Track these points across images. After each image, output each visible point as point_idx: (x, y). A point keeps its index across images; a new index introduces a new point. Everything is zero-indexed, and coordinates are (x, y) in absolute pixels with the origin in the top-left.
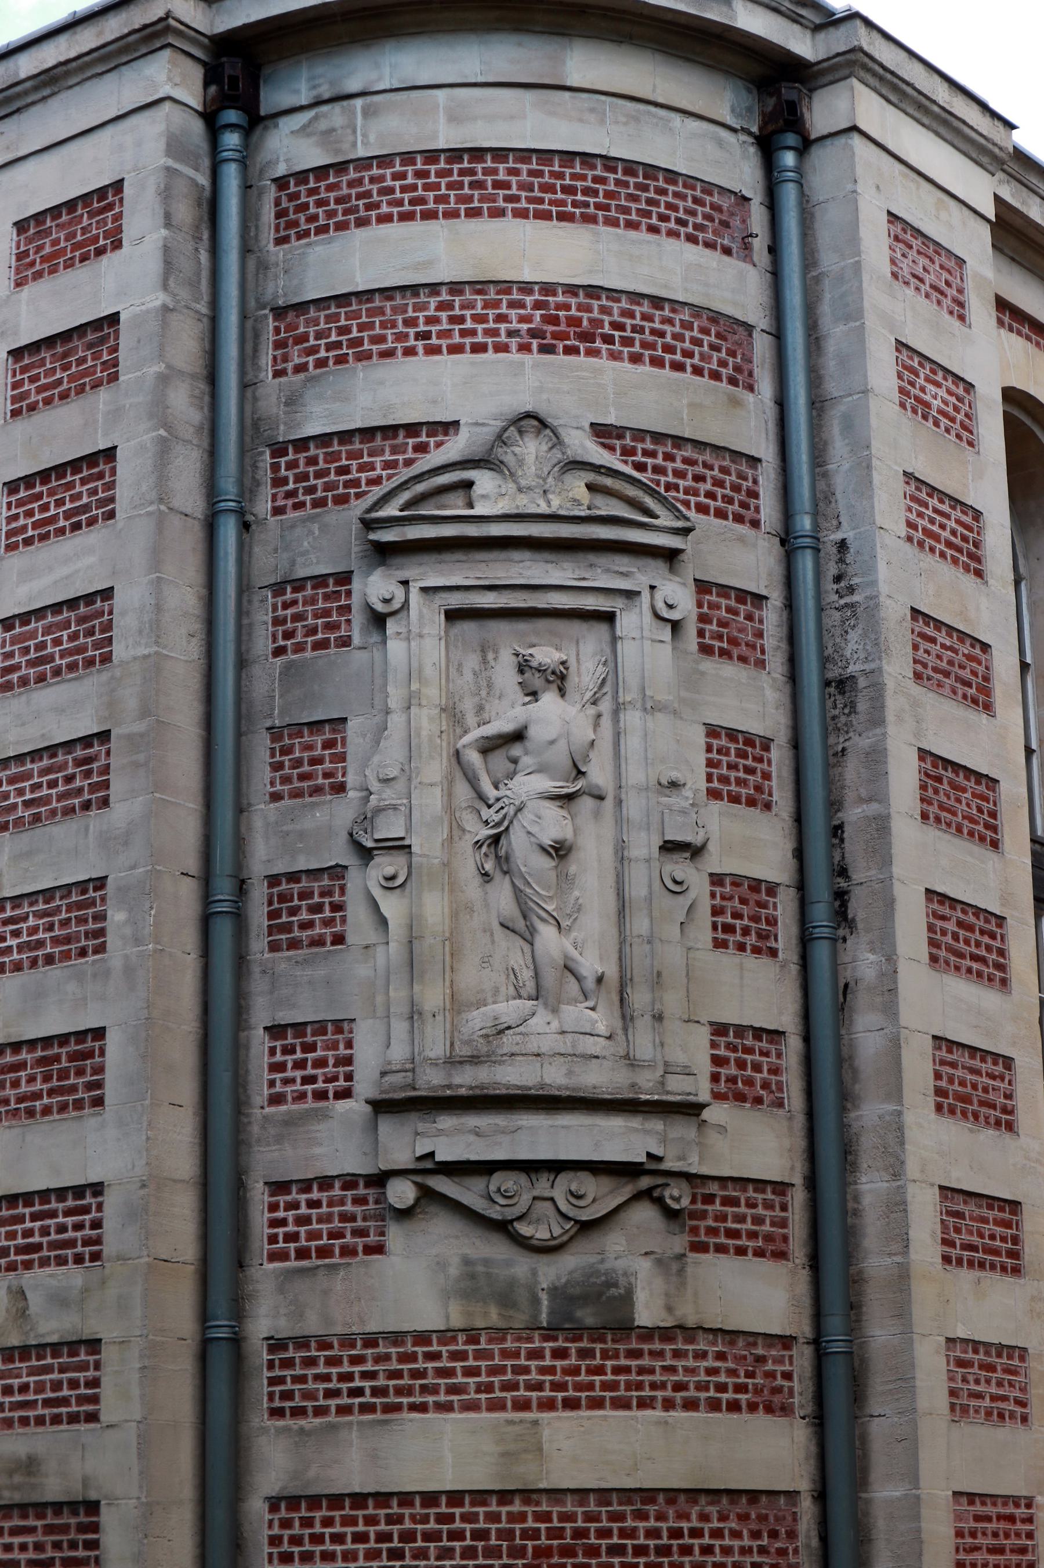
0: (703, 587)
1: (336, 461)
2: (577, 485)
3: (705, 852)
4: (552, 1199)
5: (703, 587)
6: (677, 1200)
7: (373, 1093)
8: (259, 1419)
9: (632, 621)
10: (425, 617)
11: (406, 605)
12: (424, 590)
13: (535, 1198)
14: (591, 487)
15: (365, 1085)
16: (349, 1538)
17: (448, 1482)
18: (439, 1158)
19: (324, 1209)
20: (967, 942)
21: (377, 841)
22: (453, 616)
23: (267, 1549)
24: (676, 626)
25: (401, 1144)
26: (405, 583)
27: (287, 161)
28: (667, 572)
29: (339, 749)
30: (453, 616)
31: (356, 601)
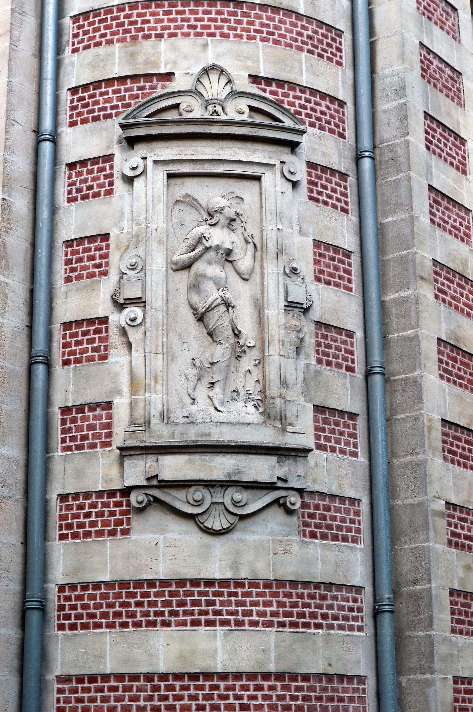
0: (311, 165)
1: (71, 247)
2: (243, 104)
3: (311, 310)
4: (223, 504)
5: (311, 165)
6: (293, 504)
7: (120, 444)
8: (53, 631)
9: (270, 179)
10: (157, 177)
11: (144, 172)
12: (155, 162)
13: (212, 503)
14: (252, 109)
15: (118, 439)
16: (106, 689)
17: (162, 668)
18: (160, 478)
19: (121, 35)
20: (453, 367)
21: (125, 299)
22: (170, 176)
23: (56, 696)
24: (295, 184)
25: (136, 472)
26: (145, 158)
27: (400, 549)
28: (290, 152)
29: (103, 268)
30: (170, 176)
31: (116, 172)
